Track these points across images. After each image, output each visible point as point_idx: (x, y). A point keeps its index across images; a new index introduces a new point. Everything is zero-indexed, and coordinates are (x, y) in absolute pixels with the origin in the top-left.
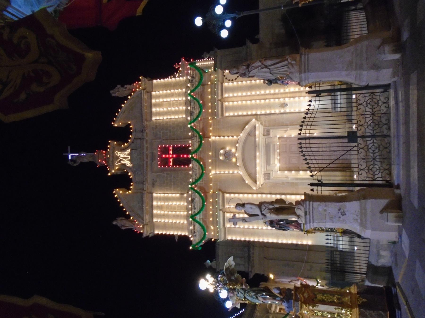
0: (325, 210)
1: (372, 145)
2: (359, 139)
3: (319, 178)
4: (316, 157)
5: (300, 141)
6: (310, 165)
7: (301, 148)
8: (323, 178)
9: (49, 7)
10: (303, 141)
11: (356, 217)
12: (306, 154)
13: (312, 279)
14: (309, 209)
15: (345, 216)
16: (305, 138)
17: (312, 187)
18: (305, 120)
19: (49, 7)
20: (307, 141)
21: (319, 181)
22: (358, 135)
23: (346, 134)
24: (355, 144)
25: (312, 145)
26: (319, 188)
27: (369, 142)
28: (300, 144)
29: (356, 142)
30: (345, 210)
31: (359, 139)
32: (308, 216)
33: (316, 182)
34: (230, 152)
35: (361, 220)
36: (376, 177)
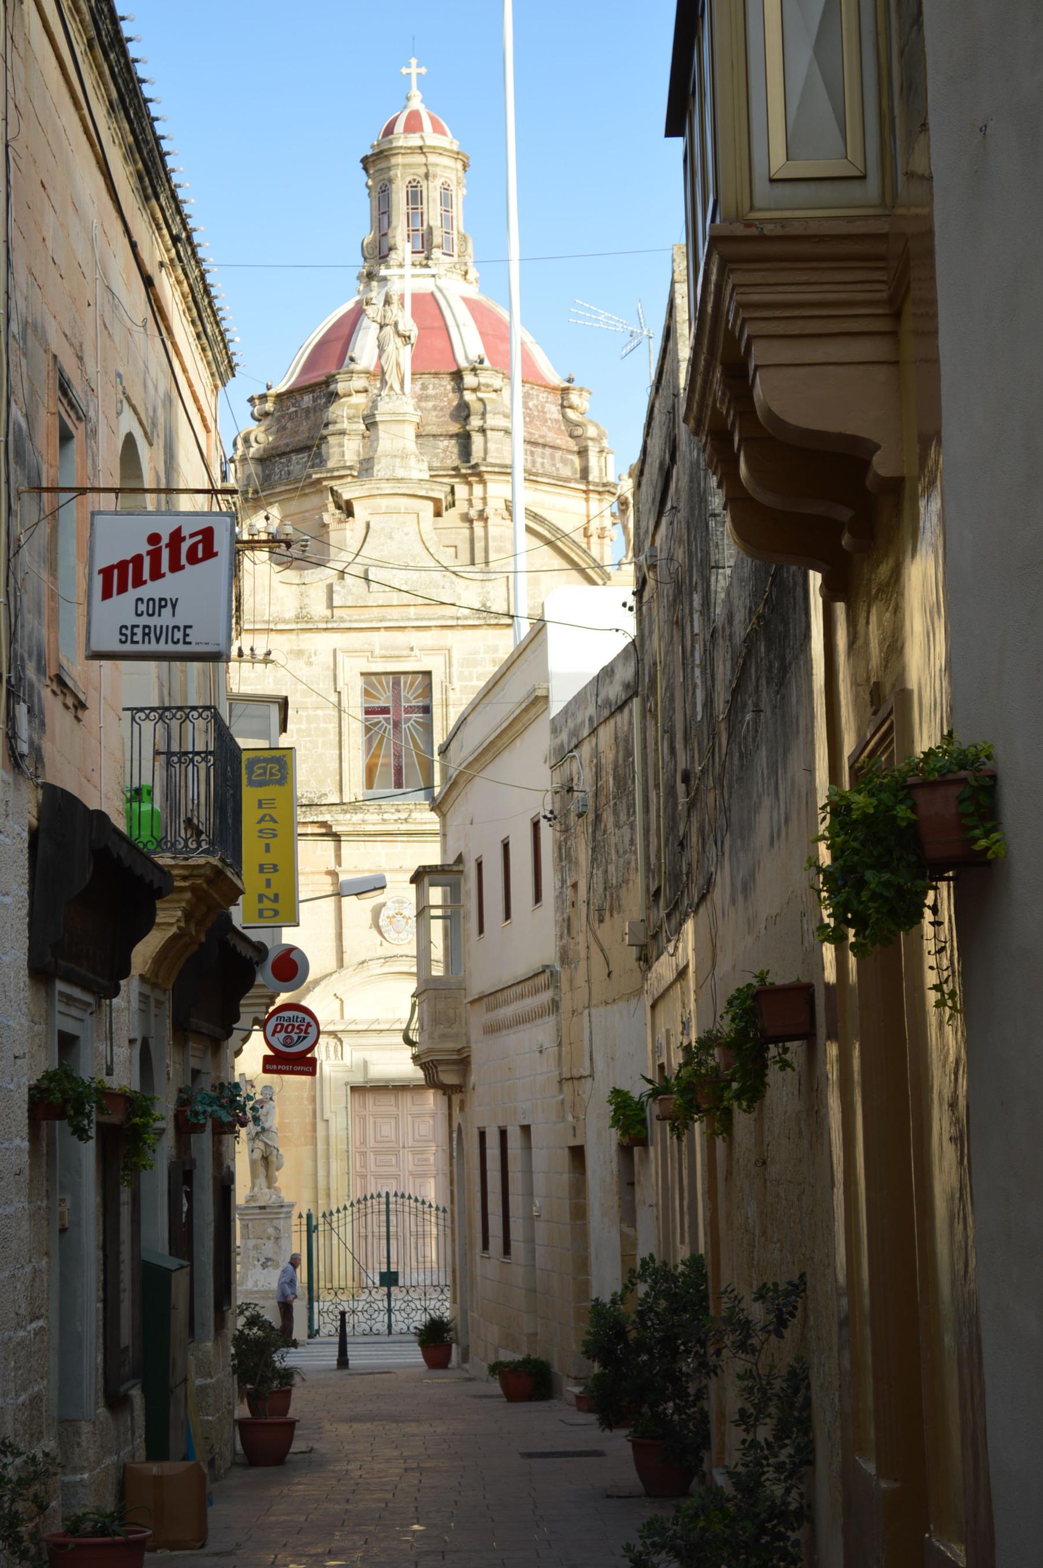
0: (269, 1238)
1: (403, 1313)
2: (385, 1289)
3: (321, 1228)
4: (349, 1227)
5: (384, 1195)
6: (336, 1215)
7: (403, 1196)
8: (321, 1234)
9: (392, 871)
10: (383, 1200)
11: (260, 1284)
12: (362, 1206)
13: (101, 1219)
14: (270, 1213)
15: (260, 1268)
16: (388, 1204)
17: (305, 1216)
18: (412, 1201)
19: (392, 871)
20: (383, 1207)
21: (316, 1227)
22: (392, 1288)
23: (393, 1269)
24: (377, 1283)
25: (400, 1215)
26: (304, 1228)
27: (380, 1304)
28: (379, 1196)
29: (381, 1285)
30: (271, 1269)
31: (385, 1289)
32: (257, 1211)
33: (314, 1223)
34: (144, 1167)
35: (257, 1292)
36: (325, 1314)
